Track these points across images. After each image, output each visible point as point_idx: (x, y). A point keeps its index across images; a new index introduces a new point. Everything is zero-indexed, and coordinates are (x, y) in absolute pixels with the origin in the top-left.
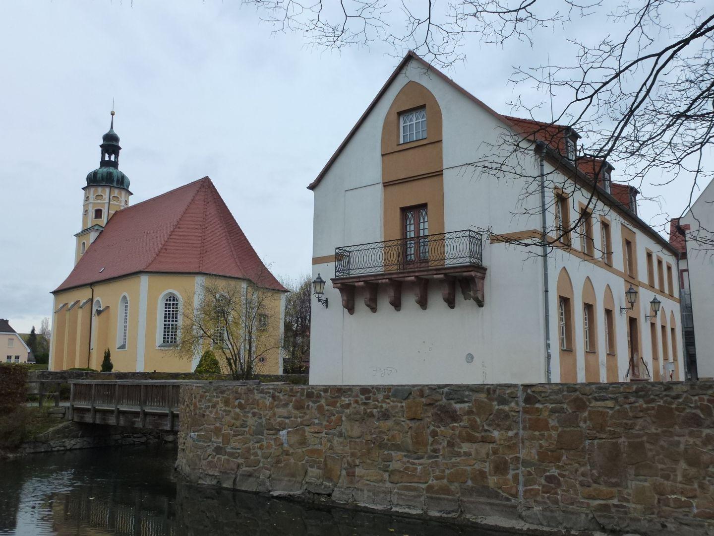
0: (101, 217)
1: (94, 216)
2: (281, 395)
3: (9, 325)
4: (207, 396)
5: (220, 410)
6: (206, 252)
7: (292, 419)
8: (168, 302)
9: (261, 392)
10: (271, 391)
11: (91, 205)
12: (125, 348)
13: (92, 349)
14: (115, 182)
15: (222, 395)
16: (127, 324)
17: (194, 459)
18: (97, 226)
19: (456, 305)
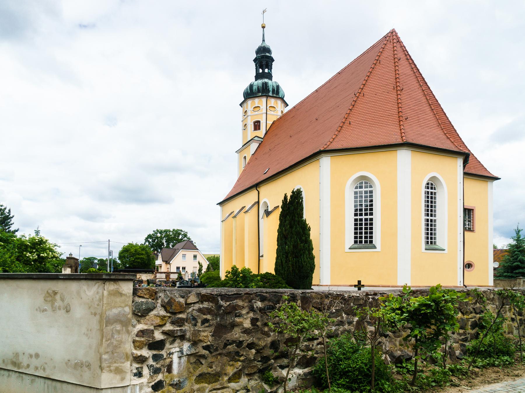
0: (259, 129)
6: (406, 119)
11: (249, 118)
13: (262, 256)
18: (256, 137)
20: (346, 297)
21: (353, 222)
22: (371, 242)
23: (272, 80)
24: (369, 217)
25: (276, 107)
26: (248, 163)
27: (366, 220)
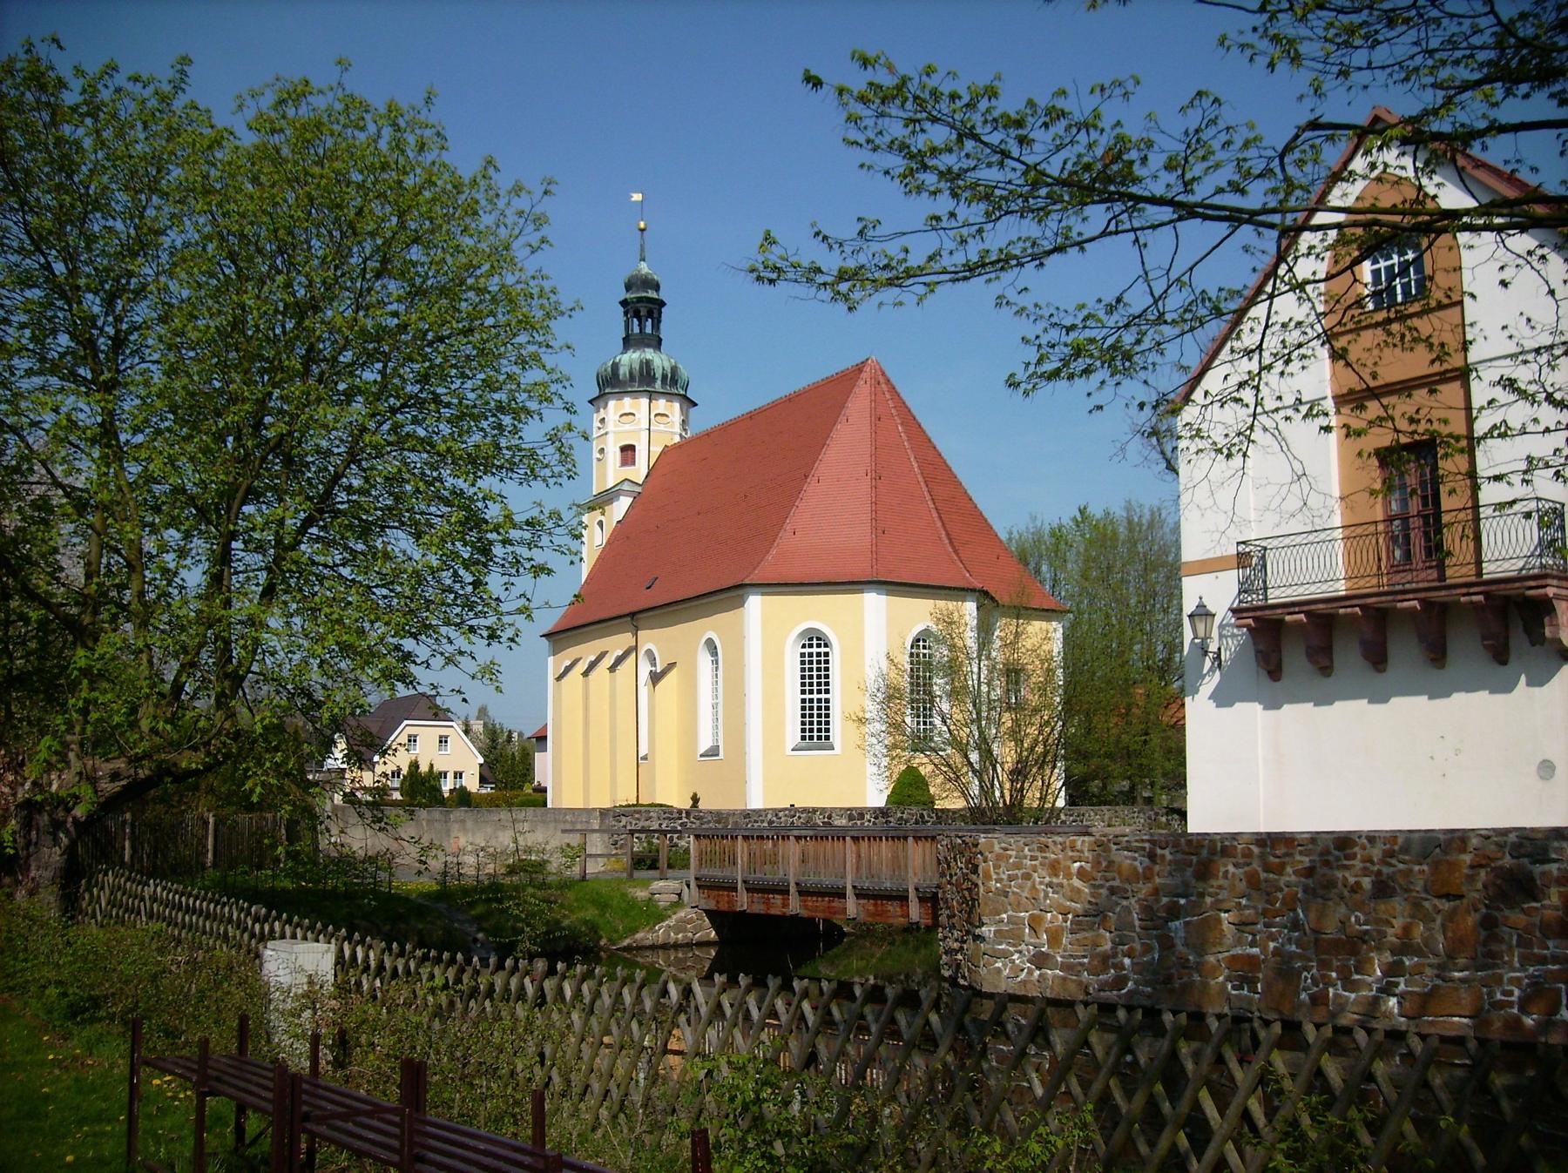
1: (618, 462)
2: (1166, 852)
4: (1010, 856)
5: (1041, 883)
7: (1193, 898)
8: (807, 650)
14: (659, 382)
19: (1512, 658)
20: (1213, 982)
21: (799, 705)
22: (827, 738)
24: (823, 696)
27: (819, 701)
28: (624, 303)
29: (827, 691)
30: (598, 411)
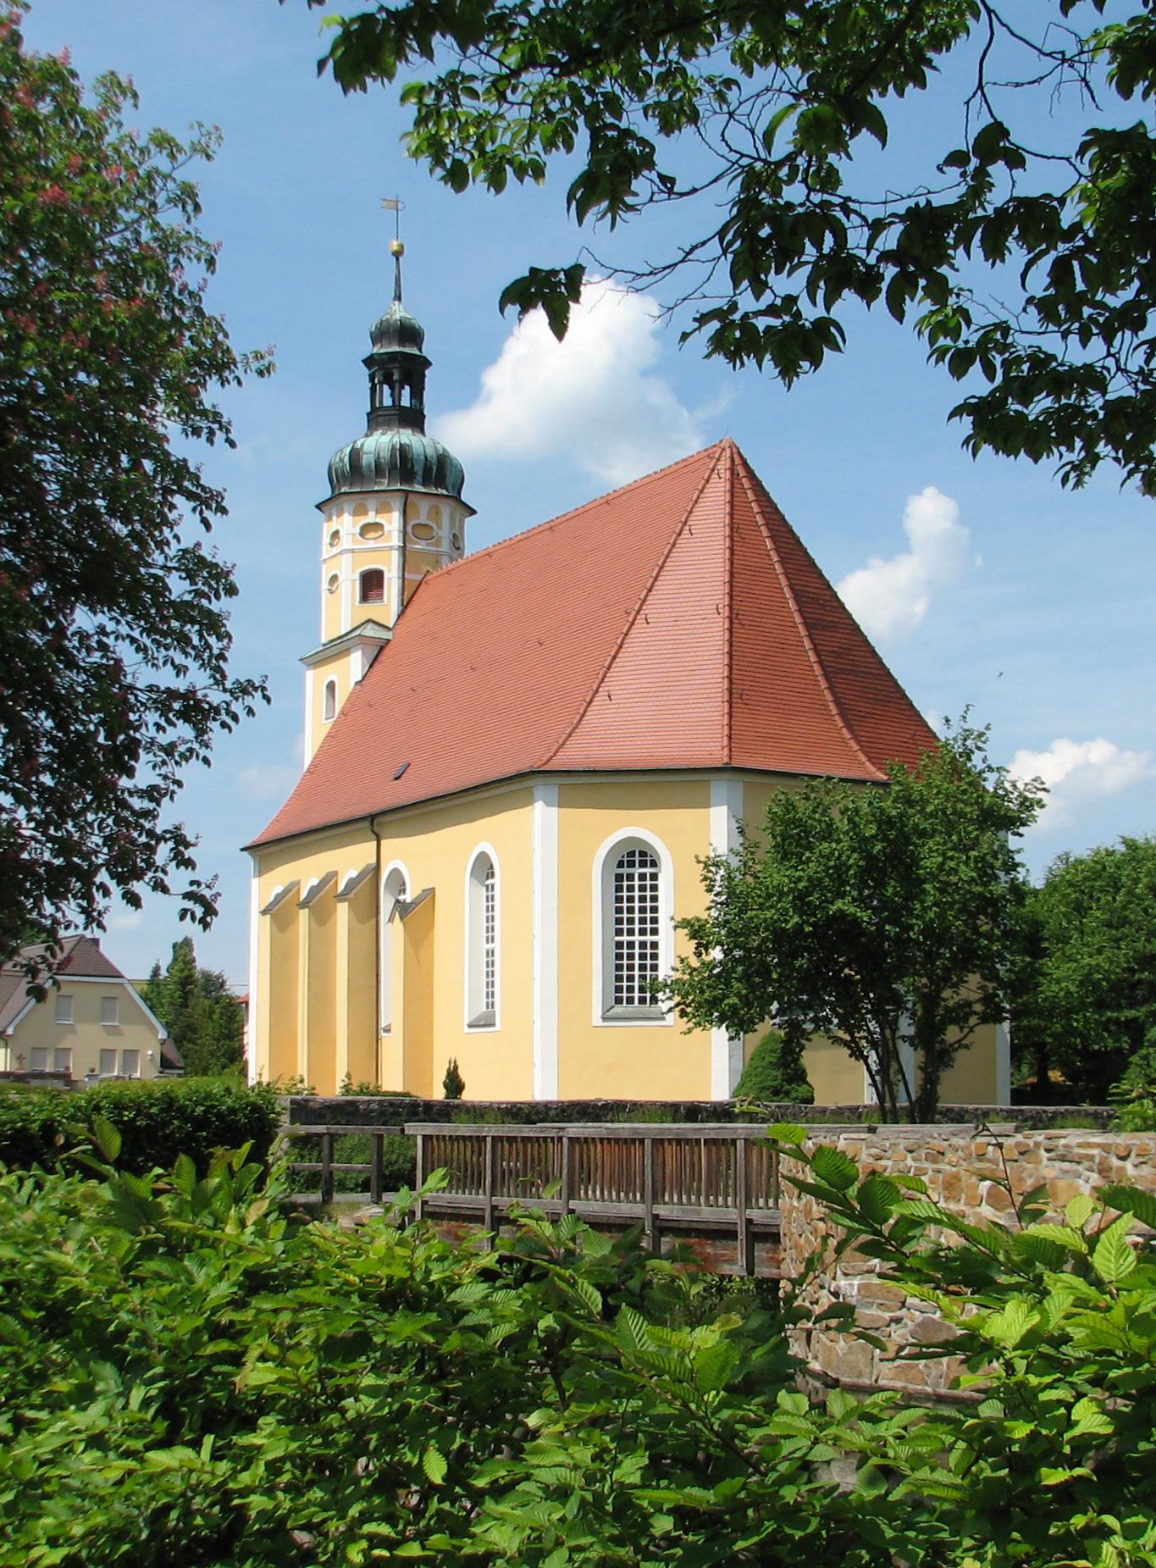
3: (102, 956)
9: (1063, 1159)
10: (1095, 1152)
12: (493, 1025)
13: (387, 1030)
15: (936, 1166)
16: (496, 945)
17: (851, 1357)
18: (370, 625)
23: (422, 431)
24: (649, 938)
25: (434, 526)
26: (343, 713)
28: (369, 362)
29: (619, 945)
30: (329, 519)
